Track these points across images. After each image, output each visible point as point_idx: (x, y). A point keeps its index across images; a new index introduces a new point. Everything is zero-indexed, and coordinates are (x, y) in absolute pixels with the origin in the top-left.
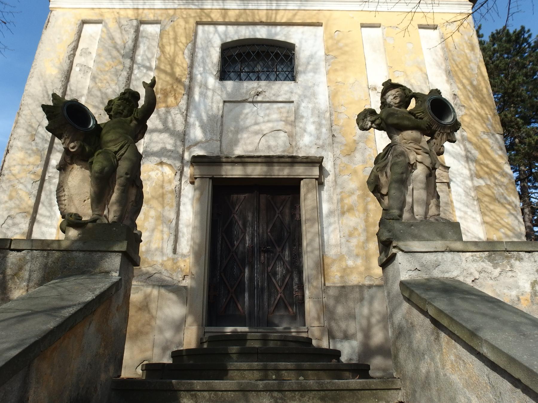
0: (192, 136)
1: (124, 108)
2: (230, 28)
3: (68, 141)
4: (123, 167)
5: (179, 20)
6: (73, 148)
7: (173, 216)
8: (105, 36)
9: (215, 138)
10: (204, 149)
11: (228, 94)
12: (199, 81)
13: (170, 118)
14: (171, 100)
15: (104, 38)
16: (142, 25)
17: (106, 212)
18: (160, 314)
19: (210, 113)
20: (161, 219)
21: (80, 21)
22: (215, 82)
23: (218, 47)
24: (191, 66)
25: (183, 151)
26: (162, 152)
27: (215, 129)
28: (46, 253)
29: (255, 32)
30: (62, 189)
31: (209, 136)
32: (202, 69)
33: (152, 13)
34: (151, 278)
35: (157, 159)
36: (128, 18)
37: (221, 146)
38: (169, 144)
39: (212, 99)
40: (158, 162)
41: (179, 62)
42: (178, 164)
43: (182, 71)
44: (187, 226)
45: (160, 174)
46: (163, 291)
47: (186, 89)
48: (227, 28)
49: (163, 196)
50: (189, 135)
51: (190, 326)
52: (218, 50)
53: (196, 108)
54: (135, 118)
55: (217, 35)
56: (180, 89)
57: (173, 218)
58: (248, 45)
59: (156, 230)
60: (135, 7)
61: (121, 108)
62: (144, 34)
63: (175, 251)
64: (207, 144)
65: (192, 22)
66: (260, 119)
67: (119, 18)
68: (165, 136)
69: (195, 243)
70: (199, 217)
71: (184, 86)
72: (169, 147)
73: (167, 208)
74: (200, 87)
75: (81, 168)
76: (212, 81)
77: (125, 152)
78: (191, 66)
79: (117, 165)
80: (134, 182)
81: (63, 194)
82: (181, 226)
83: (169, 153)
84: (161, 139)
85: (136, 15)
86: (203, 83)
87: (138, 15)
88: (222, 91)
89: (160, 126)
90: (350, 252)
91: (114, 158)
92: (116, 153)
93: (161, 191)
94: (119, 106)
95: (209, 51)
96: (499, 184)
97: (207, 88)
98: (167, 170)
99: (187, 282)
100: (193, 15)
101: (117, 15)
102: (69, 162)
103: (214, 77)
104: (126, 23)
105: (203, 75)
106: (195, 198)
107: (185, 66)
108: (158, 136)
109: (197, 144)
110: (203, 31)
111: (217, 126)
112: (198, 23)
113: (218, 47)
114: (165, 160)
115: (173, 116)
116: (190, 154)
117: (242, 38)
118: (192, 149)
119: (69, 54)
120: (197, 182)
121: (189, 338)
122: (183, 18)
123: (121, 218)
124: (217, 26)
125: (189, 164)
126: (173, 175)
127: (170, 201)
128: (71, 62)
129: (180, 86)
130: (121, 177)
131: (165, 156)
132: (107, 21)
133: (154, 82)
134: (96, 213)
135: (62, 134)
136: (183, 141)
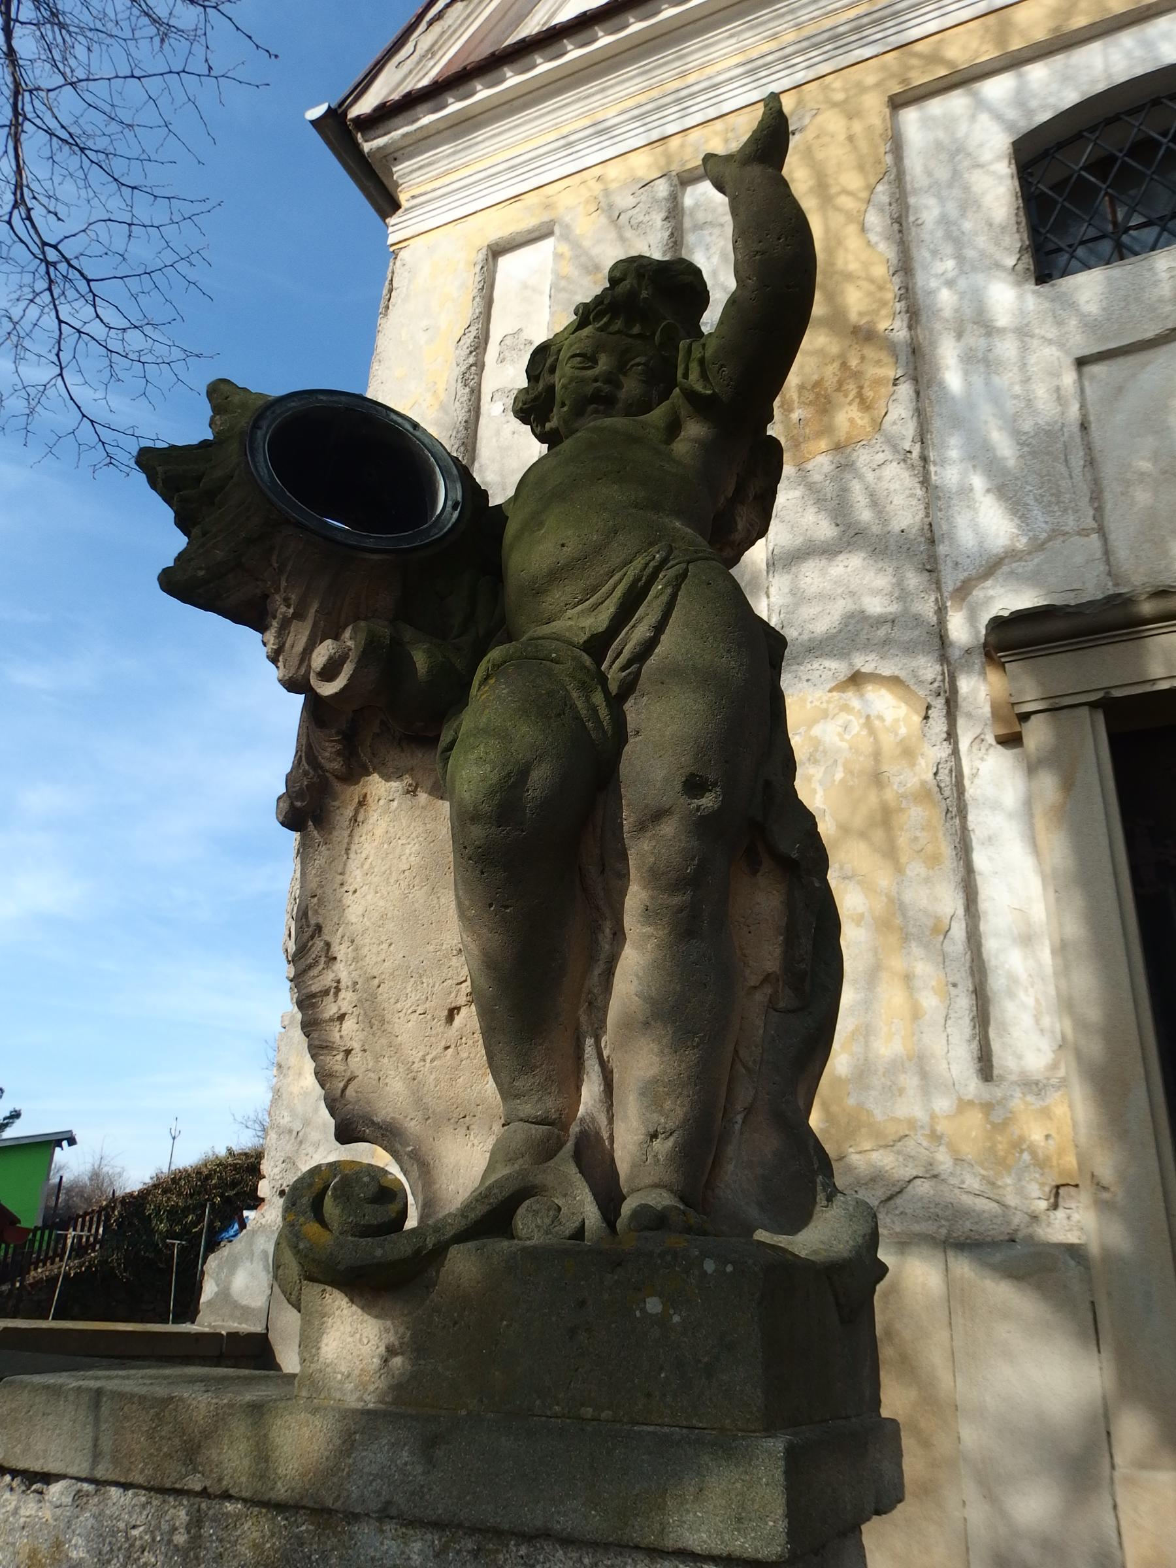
0: (966, 538)
1: (622, 366)
2: (1037, 72)
3: (299, 636)
4: (661, 736)
5: (820, 118)
6: (328, 673)
7: (949, 903)
8: (568, 269)
9: (1070, 523)
10: (1034, 579)
11: (1090, 326)
12: (947, 313)
13: (856, 487)
14: (847, 417)
15: (565, 278)
16: (689, 189)
17: (590, 1092)
19: (1027, 426)
21: (484, 251)
22: (1021, 297)
23: (998, 158)
24: (905, 267)
25: (941, 611)
26: (855, 633)
27: (1065, 484)
28: (182, 1516)
29: (1148, 45)
30: (319, 944)
31: (1041, 521)
32: (950, 264)
33: (716, 133)
34: (898, 1201)
35: (836, 668)
36: (635, 180)
37: (1107, 553)
38: (876, 592)
39: (1023, 366)
40: (842, 677)
41: (853, 266)
42: (929, 669)
43: (869, 294)
44: (1026, 940)
45: (856, 726)
46: (963, 1268)
47: (903, 358)
48: (1020, 76)
50: (951, 537)
51: (1142, 1465)
53: (957, 422)
54: (691, 396)
55: (984, 118)
56: (878, 362)
57: (949, 911)
58: (1133, 111)
59: (884, 976)
60: (655, 135)
61: (604, 363)
62: (701, 217)
64: (1038, 559)
65: (874, 105)
67: (607, 192)
69: (1080, 1024)
70: (1078, 901)
71: (891, 348)
72: (876, 606)
73: (916, 869)
74: (959, 336)
75: (412, 791)
76: (1006, 297)
77: (660, 628)
78: (905, 267)
79: (620, 734)
81: (328, 979)
82: (991, 945)
83: (882, 632)
84: (837, 582)
85: (662, 162)
86: (968, 312)
87: (669, 158)
88: (1060, 323)
89: (824, 529)
91: (585, 688)
92: (598, 645)
93: (873, 799)
94: (588, 359)
95: (967, 189)
97: (989, 329)
98: (886, 706)
99: (1074, 1224)
100: (870, 80)
101: (597, 188)
102: (336, 765)
103: (1011, 278)
104: (631, 201)
105: (962, 283)
106: (1038, 810)
107: (880, 271)
108: (823, 572)
109: (993, 566)
110: (926, 122)
112: (897, 103)
113: (998, 158)
114: (866, 663)
115: (870, 477)
116: (972, 618)
117: (1101, 87)
118: (978, 594)
119: (463, 369)
120: (1037, 734)
122: (834, 105)
123: (699, 1148)
124: (977, 85)
125: (978, 660)
126: (917, 719)
127: (923, 836)
128: (472, 391)
129: (870, 352)
130: (659, 815)
131: (867, 646)
132: (567, 219)
133: (772, 136)
134: (528, 1108)
135: (266, 597)
136: (931, 569)
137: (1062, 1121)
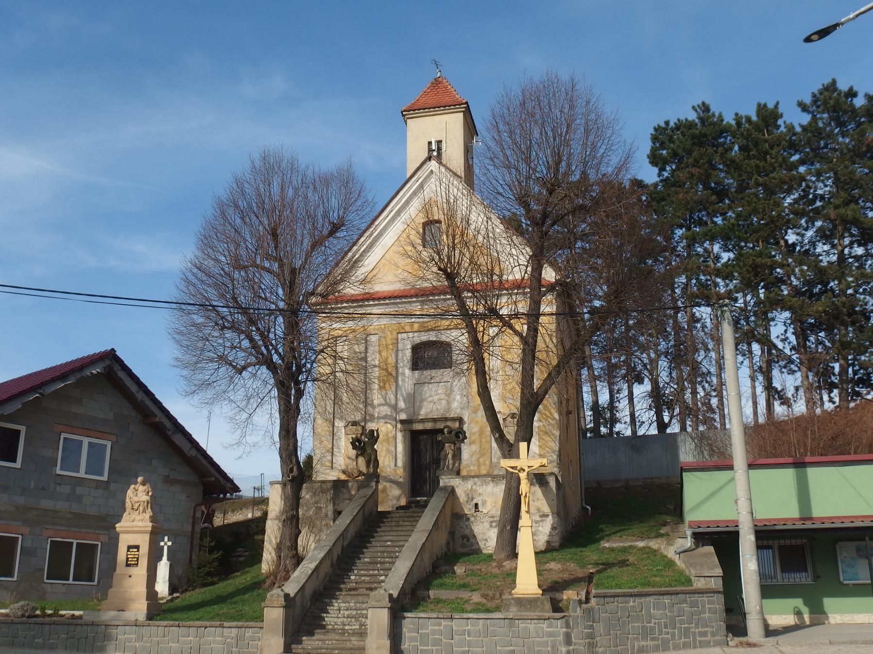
4: (373, 457)
7: (393, 449)
18: (390, 494)
20: (388, 451)
26: (385, 417)
42: (394, 423)
49: (388, 439)
52: (410, 350)
63: (396, 465)
65: (394, 333)
66: (433, 393)
68: (386, 408)
72: (389, 413)
76: (407, 372)
80: (376, 461)
90: (471, 463)
96: (550, 424)
98: (389, 426)
99: (401, 480)
111: (413, 399)
121: (403, 502)
137: (400, 472)
